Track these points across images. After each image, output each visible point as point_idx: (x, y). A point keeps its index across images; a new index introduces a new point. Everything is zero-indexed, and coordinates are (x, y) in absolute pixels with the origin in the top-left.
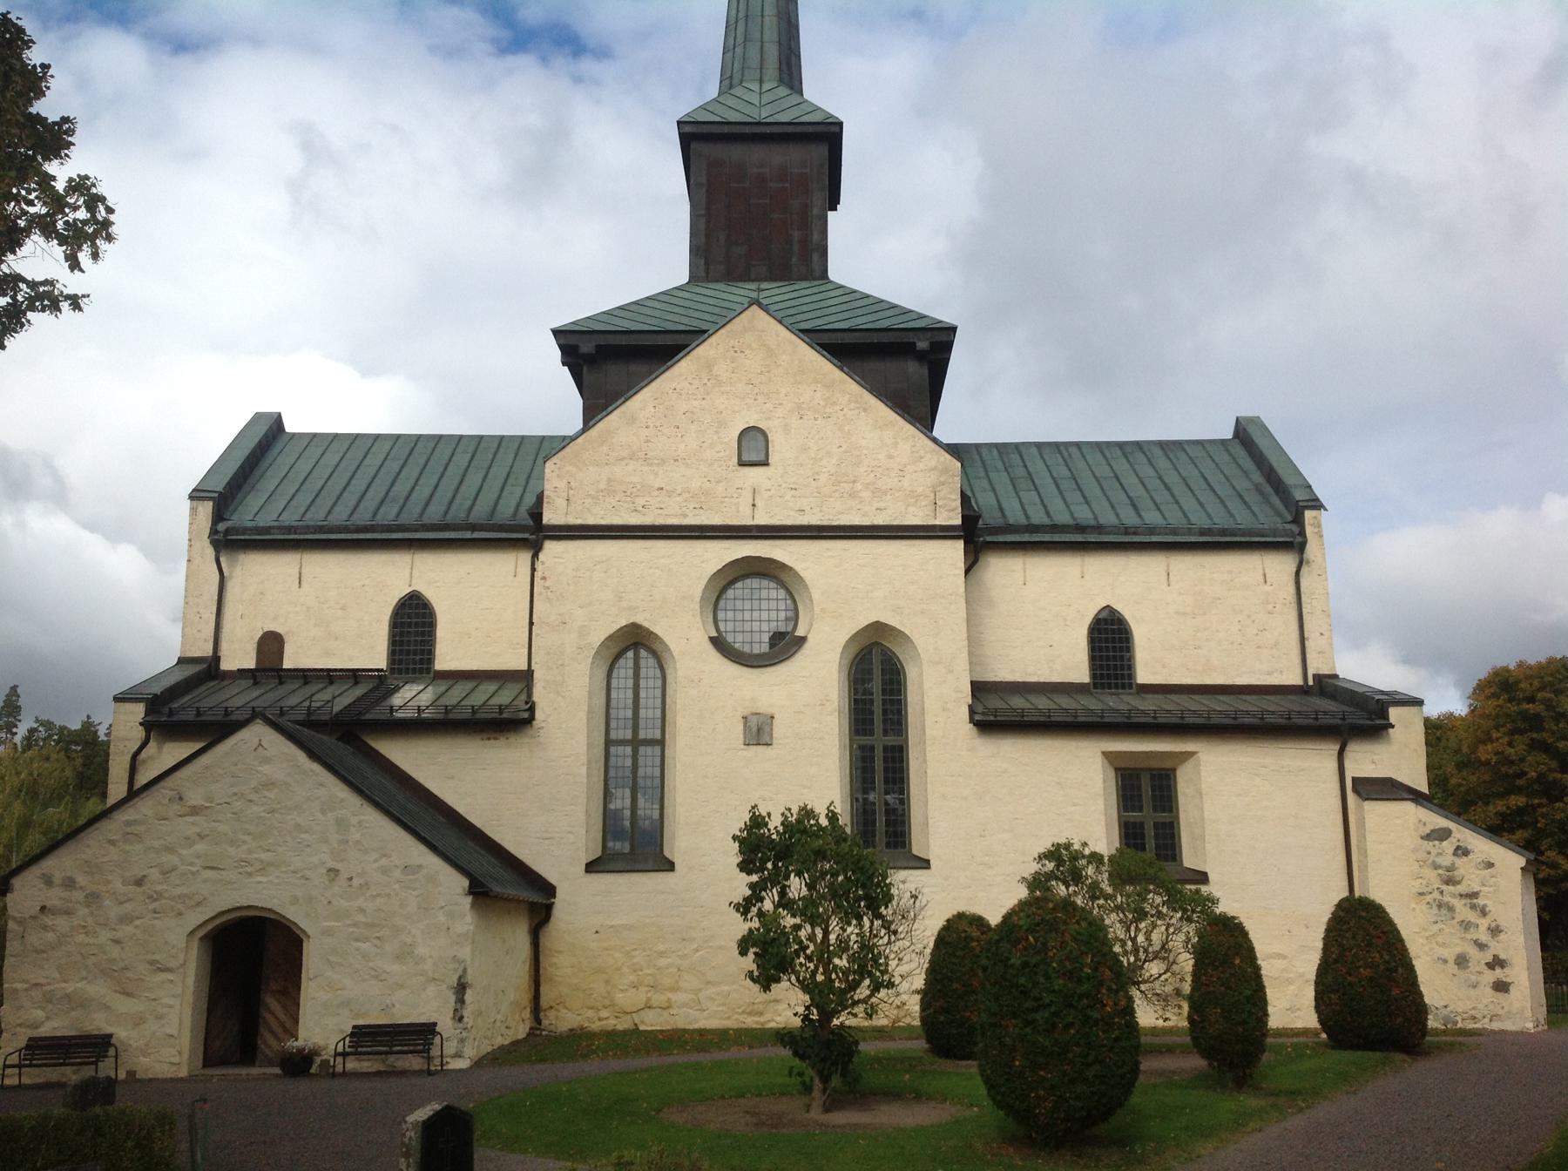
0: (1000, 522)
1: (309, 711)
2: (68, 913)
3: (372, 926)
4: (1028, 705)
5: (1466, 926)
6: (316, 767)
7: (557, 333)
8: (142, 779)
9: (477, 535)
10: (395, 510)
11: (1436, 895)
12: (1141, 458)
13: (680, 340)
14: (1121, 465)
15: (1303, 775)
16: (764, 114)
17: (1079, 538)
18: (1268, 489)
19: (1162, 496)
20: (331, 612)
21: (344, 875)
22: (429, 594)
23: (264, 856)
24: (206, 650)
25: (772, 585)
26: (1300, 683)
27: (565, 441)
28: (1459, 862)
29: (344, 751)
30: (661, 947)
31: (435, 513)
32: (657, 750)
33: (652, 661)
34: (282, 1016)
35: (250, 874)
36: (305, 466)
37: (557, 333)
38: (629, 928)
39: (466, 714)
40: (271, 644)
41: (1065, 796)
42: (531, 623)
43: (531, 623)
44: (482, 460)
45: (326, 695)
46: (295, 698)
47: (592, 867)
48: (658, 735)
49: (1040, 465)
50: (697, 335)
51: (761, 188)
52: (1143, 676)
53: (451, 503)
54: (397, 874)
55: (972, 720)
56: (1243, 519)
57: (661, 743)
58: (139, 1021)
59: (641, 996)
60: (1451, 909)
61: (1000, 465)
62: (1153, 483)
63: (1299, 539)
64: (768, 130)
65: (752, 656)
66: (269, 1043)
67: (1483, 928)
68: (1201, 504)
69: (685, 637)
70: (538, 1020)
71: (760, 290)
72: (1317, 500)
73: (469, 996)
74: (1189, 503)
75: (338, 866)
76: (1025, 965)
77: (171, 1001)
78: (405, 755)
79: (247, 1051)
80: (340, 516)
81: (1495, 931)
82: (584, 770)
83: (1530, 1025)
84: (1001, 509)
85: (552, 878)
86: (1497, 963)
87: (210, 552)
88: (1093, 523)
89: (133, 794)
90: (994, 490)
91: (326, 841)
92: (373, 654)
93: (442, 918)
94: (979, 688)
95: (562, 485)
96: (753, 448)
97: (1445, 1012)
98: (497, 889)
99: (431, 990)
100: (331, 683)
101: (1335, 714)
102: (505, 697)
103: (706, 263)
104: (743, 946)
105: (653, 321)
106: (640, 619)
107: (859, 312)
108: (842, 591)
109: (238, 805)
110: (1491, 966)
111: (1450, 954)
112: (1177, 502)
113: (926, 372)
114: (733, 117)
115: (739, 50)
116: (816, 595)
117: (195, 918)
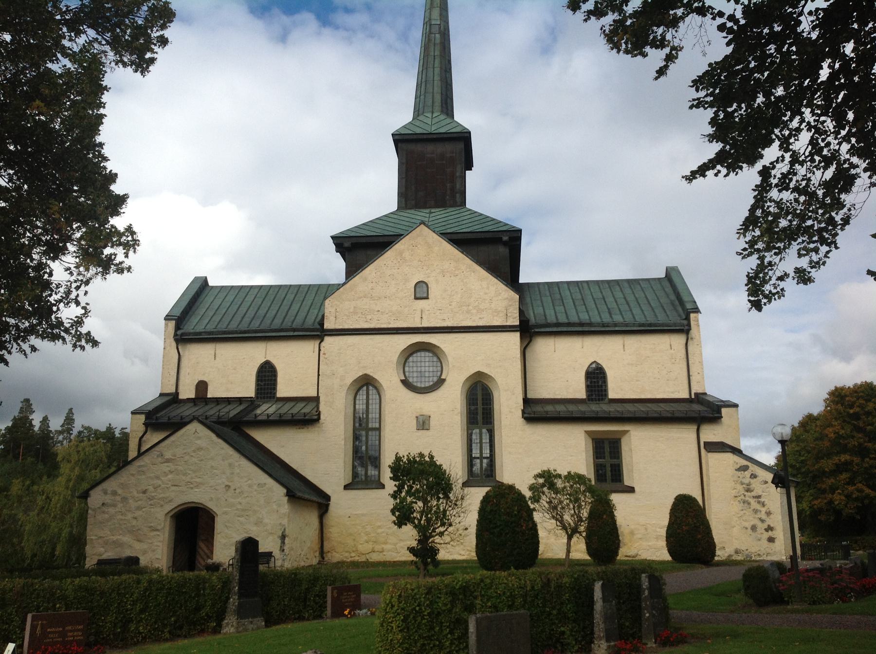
0: (543, 322)
1: (219, 417)
2: (114, 506)
3: (243, 510)
4: (598, 409)
5: (756, 511)
6: (220, 441)
7: (332, 237)
8: (143, 449)
9: (296, 333)
10: (258, 323)
11: (742, 497)
12: (618, 288)
13: (391, 239)
14: (607, 293)
15: (680, 441)
16: (433, 129)
17: (580, 329)
18: (677, 303)
19: (624, 307)
20: (230, 370)
21: (233, 488)
22: (274, 361)
23: (198, 480)
24: (172, 390)
25: (431, 355)
26: (688, 397)
27: (339, 286)
28: (752, 481)
29: (235, 436)
30: (379, 524)
31: (277, 324)
32: (377, 433)
33: (375, 391)
34: (207, 551)
35: (192, 488)
36: (217, 302)
37: (332, 237)
38: (363, 515)
39: (289, 417)
40: (202, 386)
41: (568, 451)
42: (319, 375)
43: (319, 375)
44: (300, 297)
45: (226, 410)
46: (212, 411)
47: (347, 487)
48: (377, 425)
49: (568, 293)
50: (397, 237)
51: (433, 163)
52: (612, 395)
53: (285, 318)
54: (255, 487)
55: (523, 417)
56: (662, 318)
57: (379, 429)
58: (145, 552)
59: (370, 546)
60: (749, 504)
61: (548, 294)
62: (621, 301)
63: (686, 328)
64: (435, 136)
65: (425, 388)
66: (201, 562)
67: (763, 512)
68: (642, 311)
69: (389, 380)
70: (323, 558)
71: (431, 213)
72: (697, 308)
73: (287, 540)
74: (637, 311)
75: (230, 484)
76: (492, 510)
77: (159, 544)
78: (263, 437)
79: (192, 567)
80: (233, 326)
81: (769, 513)
82: (343, 442)
83: (784, 558)
84: (545, 315)
85: (328, 491)
86: (769, 529)
87: (174, 344)
88: (588, 321)
89: (140, 454)
90: (543, 306)
91: (224, 473)
92: (248, 390)
93: (275, 507)
94: (527, 401)
95: (333, 310)
96: (421, 291)
97: (747, 552)
98: (299, 494)
99: (271, 538)
100: (229, 404)
101: (700, 411)
102: (307, 410)
103: (406, 201)
104: (393, 511)
105: (379, 231)
106: (368, 372)
107: (476, 223)
108: (464, 357)
109: (187, 458)
110: (767, 530)
111: (748, 525)
112: (631, 310)
113: (507, 250)
114: (419, 131)
115: (422, 97)
116: (450, 359)
117: (168, 507)
